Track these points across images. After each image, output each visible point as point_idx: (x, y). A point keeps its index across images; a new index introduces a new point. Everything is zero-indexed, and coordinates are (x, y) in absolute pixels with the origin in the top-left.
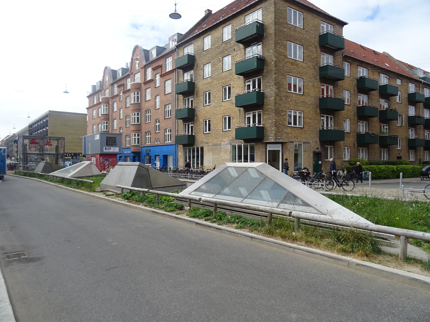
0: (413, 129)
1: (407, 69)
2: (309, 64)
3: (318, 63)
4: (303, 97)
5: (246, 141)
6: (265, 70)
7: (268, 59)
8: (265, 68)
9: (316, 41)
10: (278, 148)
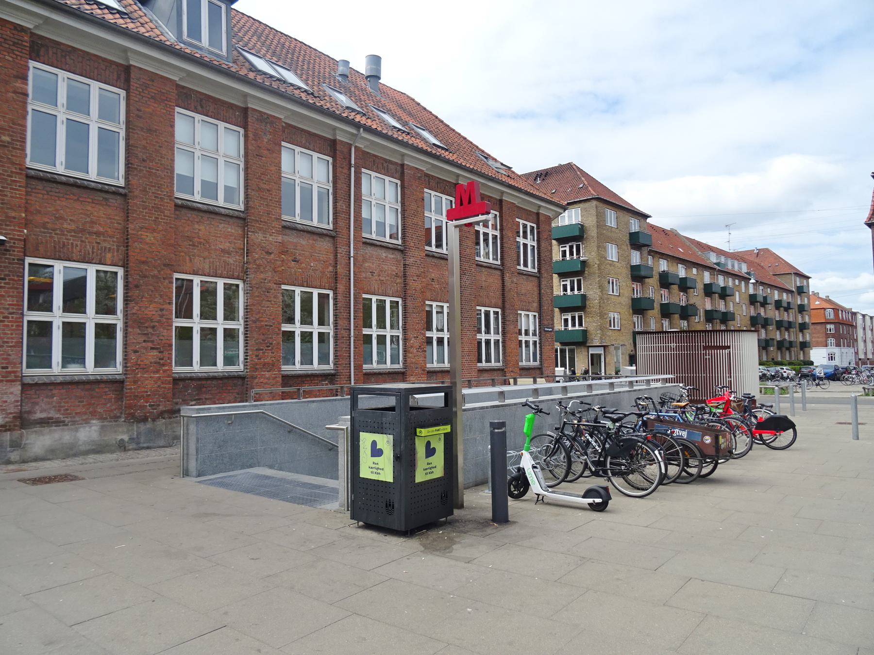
0: (638, 284)
1: (700, 253)
2: (623, 263)
3: (629, 261)
4: (620, 298)
5: (563, 344)
6: (586, 272)
7: (591, 262)
8: (586, 269)
9: (626, 238)
10: (600, 351)
